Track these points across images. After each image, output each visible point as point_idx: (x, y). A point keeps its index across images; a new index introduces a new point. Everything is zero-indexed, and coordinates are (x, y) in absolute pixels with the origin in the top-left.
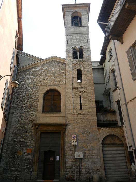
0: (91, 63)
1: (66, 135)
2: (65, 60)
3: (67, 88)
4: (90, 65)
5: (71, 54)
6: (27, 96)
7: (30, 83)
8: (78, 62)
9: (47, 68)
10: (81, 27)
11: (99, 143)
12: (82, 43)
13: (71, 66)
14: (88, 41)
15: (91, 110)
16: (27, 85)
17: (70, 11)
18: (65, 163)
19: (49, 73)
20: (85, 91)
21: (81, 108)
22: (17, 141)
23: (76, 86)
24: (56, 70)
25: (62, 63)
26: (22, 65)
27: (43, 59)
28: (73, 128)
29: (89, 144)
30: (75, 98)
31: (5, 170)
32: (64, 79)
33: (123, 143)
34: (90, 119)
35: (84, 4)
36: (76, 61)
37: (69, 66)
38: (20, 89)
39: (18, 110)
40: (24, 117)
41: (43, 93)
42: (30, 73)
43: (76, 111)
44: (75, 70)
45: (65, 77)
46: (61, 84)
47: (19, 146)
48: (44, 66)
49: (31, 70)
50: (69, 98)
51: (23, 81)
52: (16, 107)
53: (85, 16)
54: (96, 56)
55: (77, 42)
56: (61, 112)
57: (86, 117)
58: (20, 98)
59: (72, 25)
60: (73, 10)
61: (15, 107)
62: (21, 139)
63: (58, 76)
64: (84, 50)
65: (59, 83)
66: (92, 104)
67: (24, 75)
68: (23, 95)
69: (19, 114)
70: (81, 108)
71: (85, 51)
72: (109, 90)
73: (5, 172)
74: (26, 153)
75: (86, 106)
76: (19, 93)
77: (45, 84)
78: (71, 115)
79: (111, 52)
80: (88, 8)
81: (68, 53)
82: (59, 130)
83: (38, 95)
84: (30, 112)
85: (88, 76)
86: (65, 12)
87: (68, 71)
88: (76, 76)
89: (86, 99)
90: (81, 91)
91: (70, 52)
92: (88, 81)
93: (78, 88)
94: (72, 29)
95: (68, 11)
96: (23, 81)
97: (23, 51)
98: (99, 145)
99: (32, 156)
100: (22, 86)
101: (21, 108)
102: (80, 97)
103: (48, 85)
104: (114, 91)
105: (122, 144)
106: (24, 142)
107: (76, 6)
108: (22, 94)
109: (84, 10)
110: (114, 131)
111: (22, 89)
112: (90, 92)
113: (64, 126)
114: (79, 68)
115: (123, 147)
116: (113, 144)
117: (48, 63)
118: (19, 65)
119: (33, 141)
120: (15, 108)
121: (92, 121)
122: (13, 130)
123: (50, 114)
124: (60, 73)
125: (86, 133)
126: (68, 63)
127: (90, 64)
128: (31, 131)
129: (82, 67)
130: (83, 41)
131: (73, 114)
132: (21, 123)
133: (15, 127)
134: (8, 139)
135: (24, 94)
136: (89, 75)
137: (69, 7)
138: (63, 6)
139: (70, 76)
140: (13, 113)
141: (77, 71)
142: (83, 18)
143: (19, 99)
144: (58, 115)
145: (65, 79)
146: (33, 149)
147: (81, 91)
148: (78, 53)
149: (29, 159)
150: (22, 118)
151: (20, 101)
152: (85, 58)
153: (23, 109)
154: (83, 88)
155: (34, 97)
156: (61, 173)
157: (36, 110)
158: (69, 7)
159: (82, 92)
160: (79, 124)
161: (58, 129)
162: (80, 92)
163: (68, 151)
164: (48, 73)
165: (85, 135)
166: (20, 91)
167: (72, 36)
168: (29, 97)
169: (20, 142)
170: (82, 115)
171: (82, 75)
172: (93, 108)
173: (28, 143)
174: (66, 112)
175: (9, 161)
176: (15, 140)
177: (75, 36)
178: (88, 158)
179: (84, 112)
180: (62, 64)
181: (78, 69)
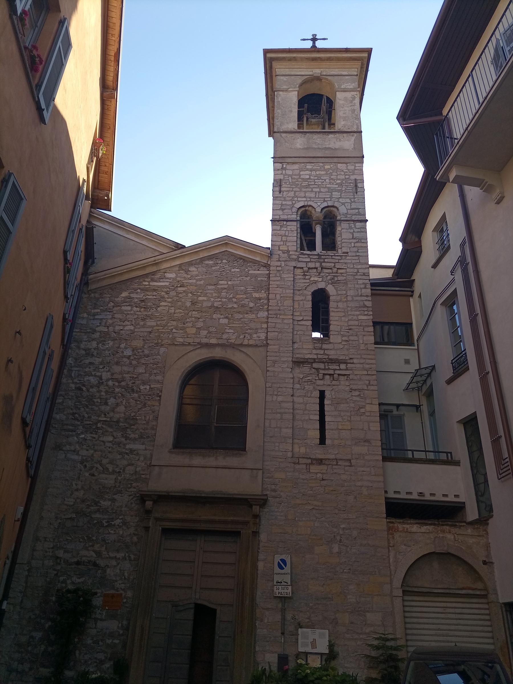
0: (366, 271)
1: (261, 544)
2: (269, 253)
3: (273, 358)
4: (364, 277)
6: (117, 384)
7: (133, 332)
8: (318, 265)
9: (200, 280)
10: (331, 136)
11: (391, 583)
12: (336, 194)
13: (288, 277)
15: (362, 449)
17: (293, 73)
19: (205, 298)
20: (339, 375)
21: (322, 440)
25: (254, 262)
30: (301, 400)
33: (486, 589)
34: (359, 484)
35: (347, 50)
36: (306, 259)
38: (93, 355)
39: (78, 435)
40: (100, 462)
41: (180, 374)
43: (303, 450)
45: (268, 318)
46: (251, 342)
48: (187, 272)
49: (136, 286)
50: (280, 399)
51: (103, 324)
53: (349, 95)
54: (384, 249)
55: (318, 190)
58: (88, 391)
59: (300, 126)
60: (307, 71)
62: (84, 553)
63: (239, 312)
64: (341, 221)
65: (242, 337)
67: (109, 303)
68: (101, 378)
69: (84, 453)
70: (322, 440)
71: (345, 225)
72: (429, 374)
74: (111, 470)
77: (190, 340)
79: (442, 231)
80: (362, 64)
81: (281, 226)
82: (233, 520)
83: (158, 382)
84: (125, 445)
85: (355, 317)
86: (274, 77)
87: (278, 297)
88: (309, 315)
89: (342, 406)
91: (289, 223)
92: (352, 338)
93: (314, 361)
94: (300, 142)
95: (287, 72)
96: (103, 324)
97: (110, 211)
98: (391, 592)
99: (125, 622)
100: (98, 344)
102: (322, 395)
104: (449, 382)
105: (483, 593)
106: (95, 564)
107: (315, 54)
110: (450, 536)
112: (360, 380)
114: (322, 285)
115: (486, 606)
116: (448, 591)
117: (202, 260)
118: (93, 262)
119: (130, 560)
120: (65, 427)
124: (246, 301)
125: (341, 541)
126: (278, 264)
127: (364, 274)
128: (125, 523)
130: (341, 185)
135: (105, 376)
136: (358, 313)
137: (290, 59)
139: (284, 315)
140: (58, 447)
141: (310, 298)
142: (341, 102)
143: (85, 394)
144: (233, 461)
145: (265, 326)
146: (129, 594)
148: (320, 225)
150: (92, 468)
153: (96, 433)
154: (332, 361)
155: (142, 387)
158: (290, 59)
159: (328, 377)
162: (321, 376)
163: (268, 609)
164: (200, 298)
165: (336, 549)
166: (91, 363)
167: (296, 167)
169: (78, 563)
170: (325, 467)
171: (331, 314)
172: (367, 441)
173: (108, 571)
176: (60, 553)
177: (309, 166)
179: (333, 457)
181: (314, 288)
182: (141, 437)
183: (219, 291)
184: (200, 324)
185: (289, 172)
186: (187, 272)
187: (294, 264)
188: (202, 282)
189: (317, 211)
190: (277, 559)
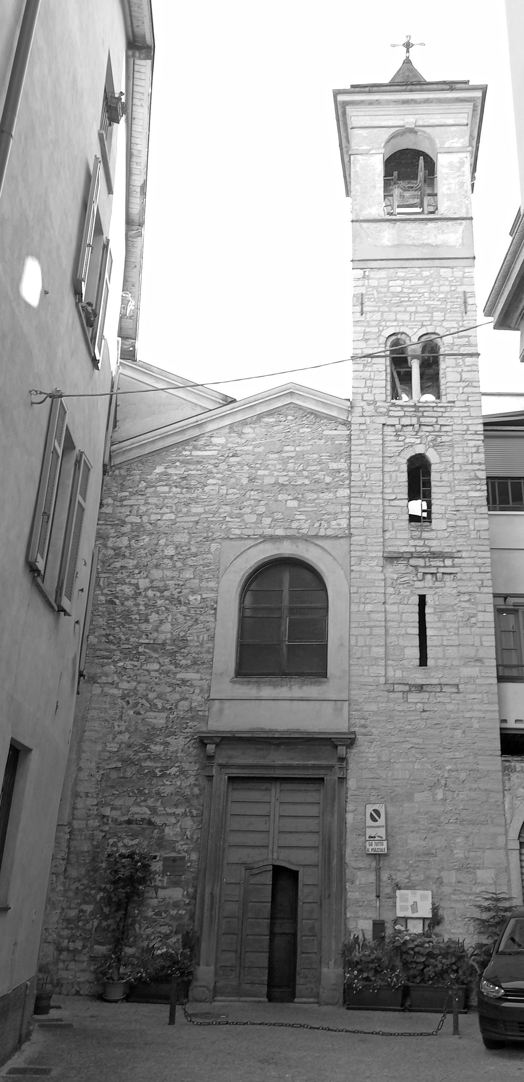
3: (358, 554)
5: (382, 367)
6: (158, 594)
8: (414, 420)
9: (258, 446)
11: (506, 834)
12: (438, 316)
13: (375, 439)
14: (465, 302)
15: (472, 671)
16: (156, 532)
17: (376, 123)
18: (345, 924)
19: (266, 472)
21: (423, 661)
22: (115, 821)
23: (399, 543)
24: (300, 456)
25: (330, 418)
26: (128, 428)
27: (234, 401)
28: (384, 759)
29: (459, 840)
30: (394, 608)
31: (65, 953)
32: (342, 505)
34: (468, 715)
37: (369, 437)
39: (115, 662)
40: (145, 697)
42: (170, 471)
43: (399, 674)
44: (399, 460)
45: (350, 497)
46: (329, 532)
47: (126, 841)
48: (240, 434)
49: (173, 457)
50: (369, 608)
52: (107, 650)
53: (455, 158)
55: (413, 309)
56: (325, 675)
57: (450, 707)
58: (123, 604)
61: (102, 647)
62: (135, 809)
65: (317, 525)
66: (477, 638)
69: (124, 685)
70: (423, 661)
73: (64, 962)
75: (451, 652)
76: (119, 576)
77: (250, 532)
78: (374, 694)
81: (365, 365)
82: (317, 763)
84: (175, 674)
85: (464, 494)
89: (448, 616)
90: (427, 570)
93: (412, 555)
94: (387, 235)
96: (134, 512)
99: (191, 890)
100: (130, 540)
101: (132, 653)
102: (422, 600)
103: (261, 536)
106: (150, 823)
108: (134, 581)
109: (450, 121)
111: (133, 555)
112: (470, 580)
113: (334, 747)
114: (419, 449)
117: (260, 417)
121: (476, 725)
122: (93, 765)
123: (258, 684)
124: (320, 475)
126: (362, 420)
128: (182, 772)
129: (436, 445)
130: (445, 300)
131: (382, 687)
132: (132, 729)
133: (104, 750)
134: (74, 808)
135: (143, 583)
136: (468, 488)
138: (341, 98)
139: (372, 492)
141: (405, 468)
143: (119, 609)
144: (311, 691)
145: (346, 509)
146: (194, 856)
147: (425, 574)
149: (176, 905)
151: (125, 619)
152: (450, 398)
154: (434, 555)
155: (191, 598)
156: (325, 970)
157: (202, 663)
159: (429, 577)
160: (415, 740)
161: (312, 762)
162: (420, 576)
163: (359, 869)
164: (260, 473)
165: (440, 796)
167: (383, 274)
168: (171, 599)
169: (129, 822)
172: (479, 660)
173: (167, 830)
174: (353, 679)
175: (82, 911)
176: (107, 811)
177: (401, 273)
178: (453, 905)
180: (333, 425)
182: (195, 663)
183: (285, 461)
184: (261, 509)
185: (374, 283)
186: (240, 434)
187: (382, 420)
188: (261, 449)
189: (413, 347)
190: (370, 809)
